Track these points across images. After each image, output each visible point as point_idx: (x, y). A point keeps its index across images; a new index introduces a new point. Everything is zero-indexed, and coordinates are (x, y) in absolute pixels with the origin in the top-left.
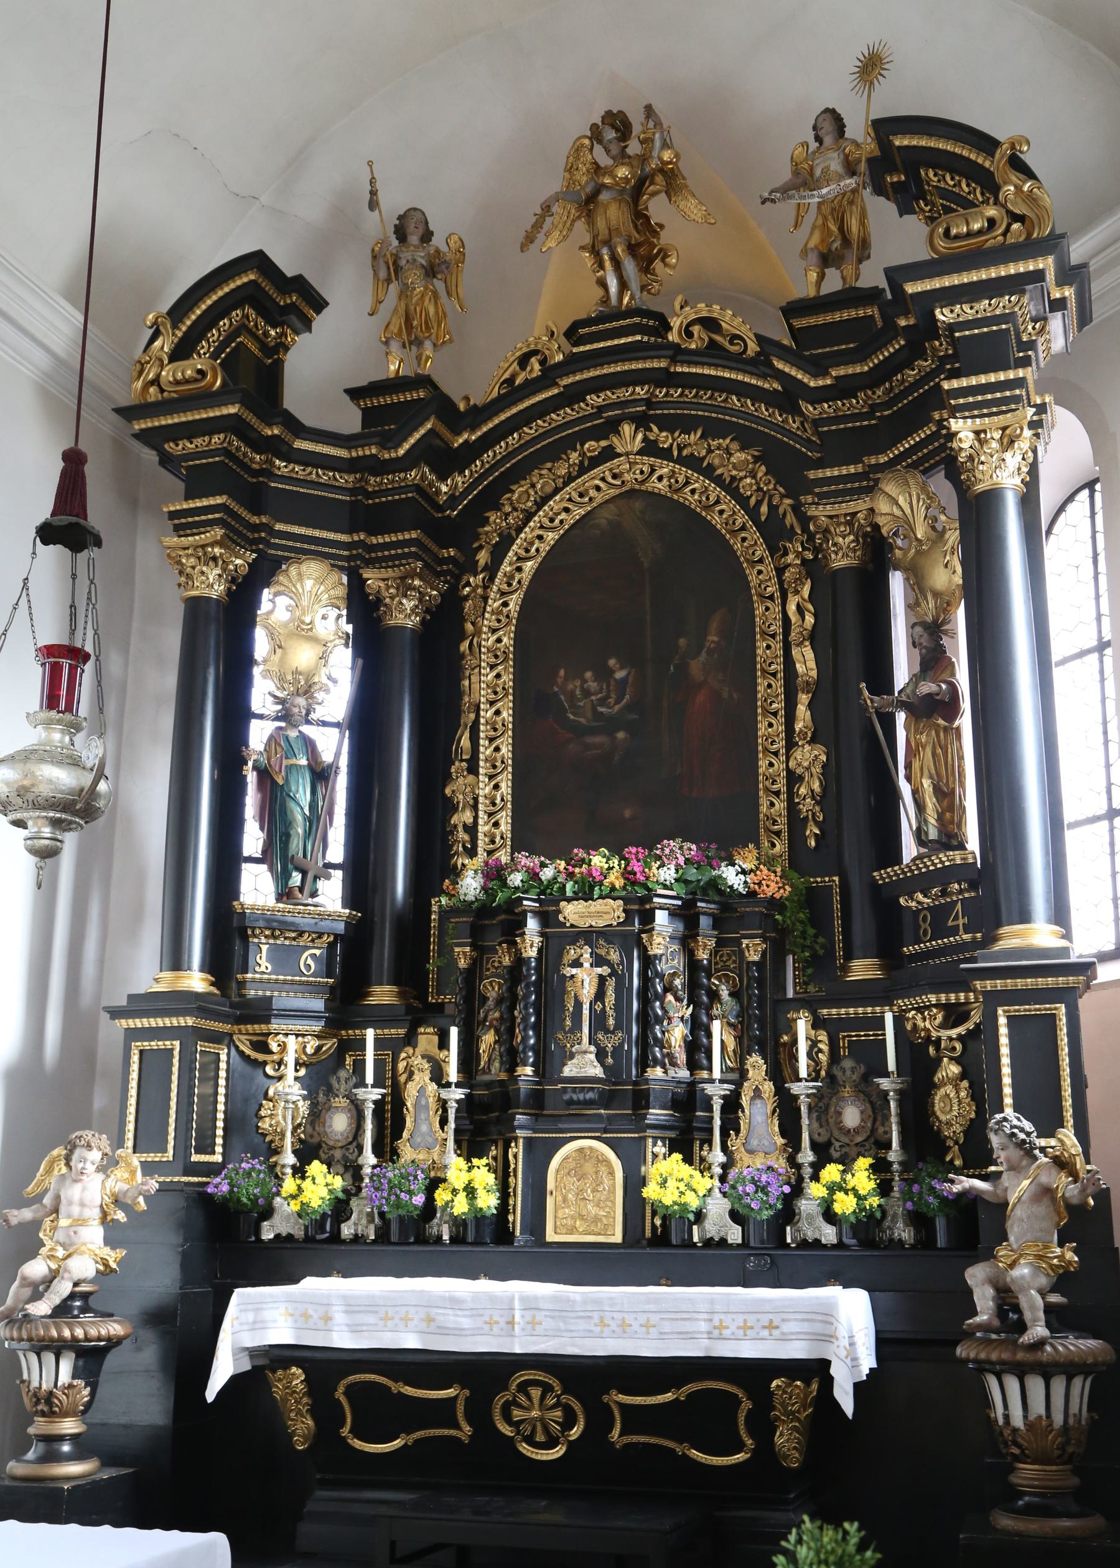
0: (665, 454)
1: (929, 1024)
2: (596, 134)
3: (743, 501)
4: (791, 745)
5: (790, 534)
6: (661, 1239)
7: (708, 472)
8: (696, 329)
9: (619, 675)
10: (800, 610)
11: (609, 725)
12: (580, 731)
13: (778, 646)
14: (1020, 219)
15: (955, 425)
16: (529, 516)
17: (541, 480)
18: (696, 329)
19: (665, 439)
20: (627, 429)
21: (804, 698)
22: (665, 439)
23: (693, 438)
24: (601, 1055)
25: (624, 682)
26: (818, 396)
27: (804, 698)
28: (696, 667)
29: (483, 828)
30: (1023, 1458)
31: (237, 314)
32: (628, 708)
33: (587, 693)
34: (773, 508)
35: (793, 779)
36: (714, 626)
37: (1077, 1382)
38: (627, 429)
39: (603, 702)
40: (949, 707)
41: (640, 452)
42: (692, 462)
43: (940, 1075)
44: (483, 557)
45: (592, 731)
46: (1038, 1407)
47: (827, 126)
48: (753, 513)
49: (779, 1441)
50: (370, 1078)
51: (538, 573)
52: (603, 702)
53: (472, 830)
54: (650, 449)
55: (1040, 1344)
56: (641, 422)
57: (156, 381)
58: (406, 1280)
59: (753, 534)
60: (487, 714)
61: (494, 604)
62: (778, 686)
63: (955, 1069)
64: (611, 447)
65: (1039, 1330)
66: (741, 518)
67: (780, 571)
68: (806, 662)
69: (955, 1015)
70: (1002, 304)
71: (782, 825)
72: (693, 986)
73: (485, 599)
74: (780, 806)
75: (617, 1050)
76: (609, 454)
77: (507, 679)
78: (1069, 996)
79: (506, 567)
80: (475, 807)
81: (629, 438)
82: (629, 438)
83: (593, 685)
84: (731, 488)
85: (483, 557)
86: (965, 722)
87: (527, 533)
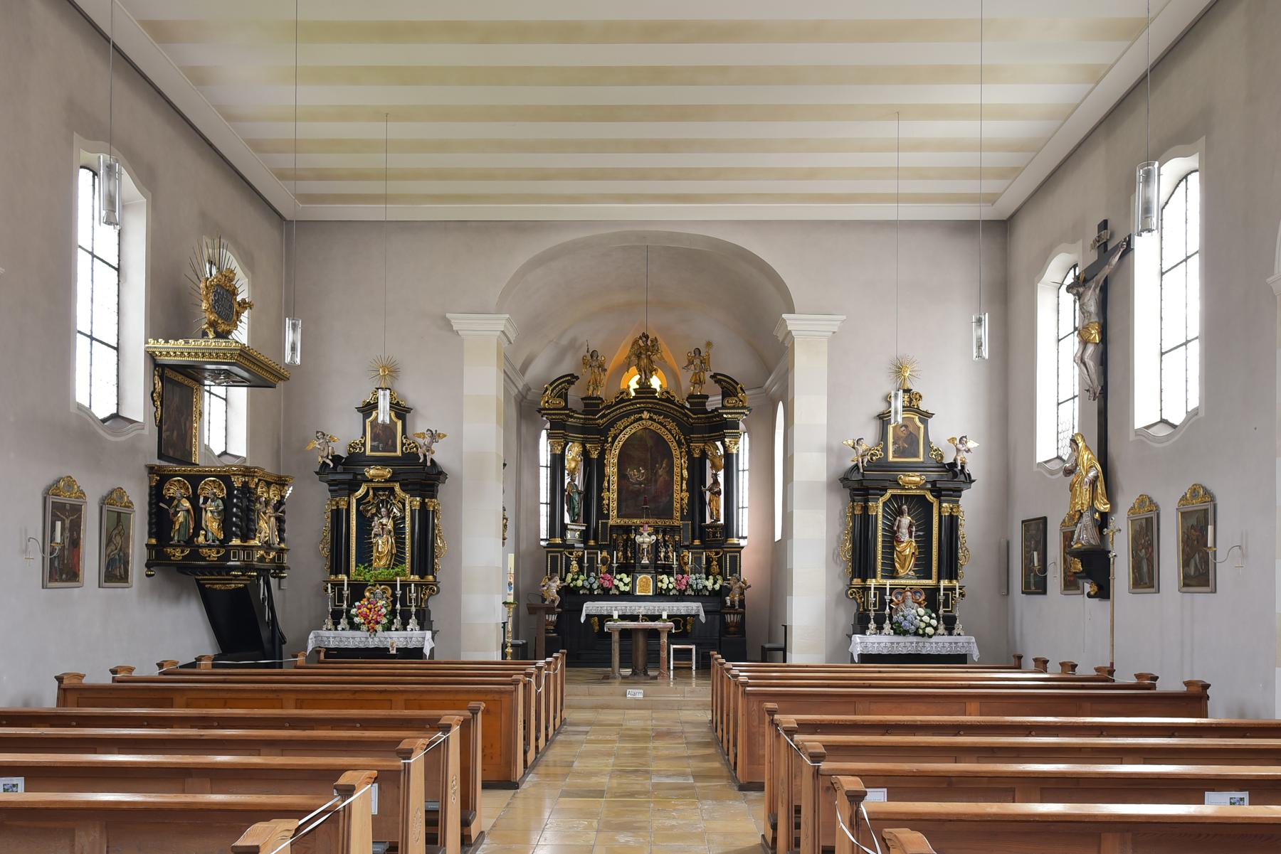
0: (654, 420)
1: (713, 555)
2: (640, 338)
3: (672, 435)
4: (681, 492)
5: (683, 444)
6: (660, 594)
7: (665, 427)
8: (664, 394)
9: (643, 471)
10: (685, 462)
11: (640, 483)
12: (634, 484)
13: (679, 470)
14: (741, 401)
15: (726, 440)
16: (622, 431)
17: (625, 422)
18: (664, 394)
19: (655, 417)
20: (645, 413)
21: (684, 482)
22: (655, 417)
23: (661, 417)
24: (648, 559)
25: (643, 473)
26: (692, 418)
27: (684, 482)
28: (660, 472)
29: (611, 505)
30: (732, 627)
31: (563, 385)
32: (644, 479)
33: (635, 475)
34: (679, 437)
35: (682, 499)
36: (664, 462)
37: (736, 616)
38: (645, 413)
39: (638, 477)
40: (719, 493)
41: (648, 419)
42: (661, 423)
43: (712, 564)
44: (610, 439)
45: (636, 484)
46: (732, 619)
47: (697, 352)
48: (675, 438)
49: (688, 628)
50: (615, 562)
51: (623, 445)
52: (638, 477)
53: (608, 505)
54: (651, 418)
55: (737, 609)
56: (649, 412)
57: (547, 402)
58: (596, 603)
59: (675, 444)
60: (611, 478)
61: (613, 452)
62: (679, 479)
63: (716, 563)
64: (641, 417)
65: (737, 607)
66: (673, 439)
67: (681, 453)
68: (685, 473)
69: (717, 553)
70: (736, 416)
71: (679, 510)
72: (665, 545)
73: (611, 450)
74: (679, 505)
75: (651, 557)
76: (641, 419)
77: (616, 470)
78: (740, 552)
79: (616, 443)
80: (609, 500)
81: (646, 415)
82: (646, 415)
83: (636, 473)
84: (670, 431)
85: (610, 439)
86: (722, 497)
87: (621, 436)
